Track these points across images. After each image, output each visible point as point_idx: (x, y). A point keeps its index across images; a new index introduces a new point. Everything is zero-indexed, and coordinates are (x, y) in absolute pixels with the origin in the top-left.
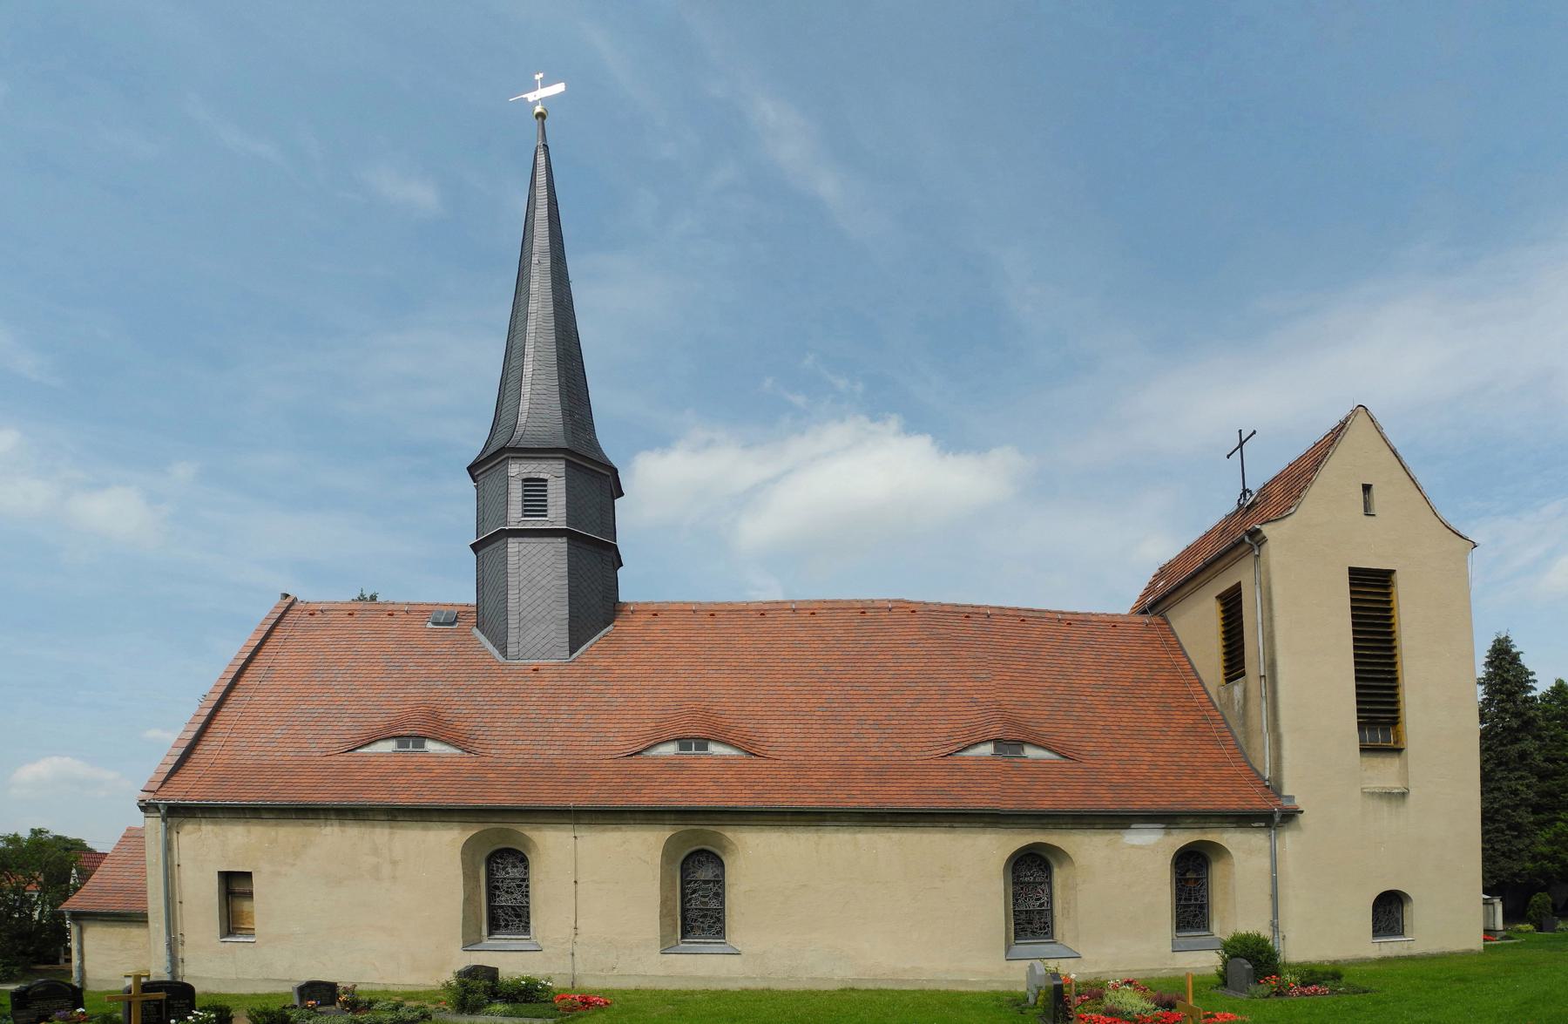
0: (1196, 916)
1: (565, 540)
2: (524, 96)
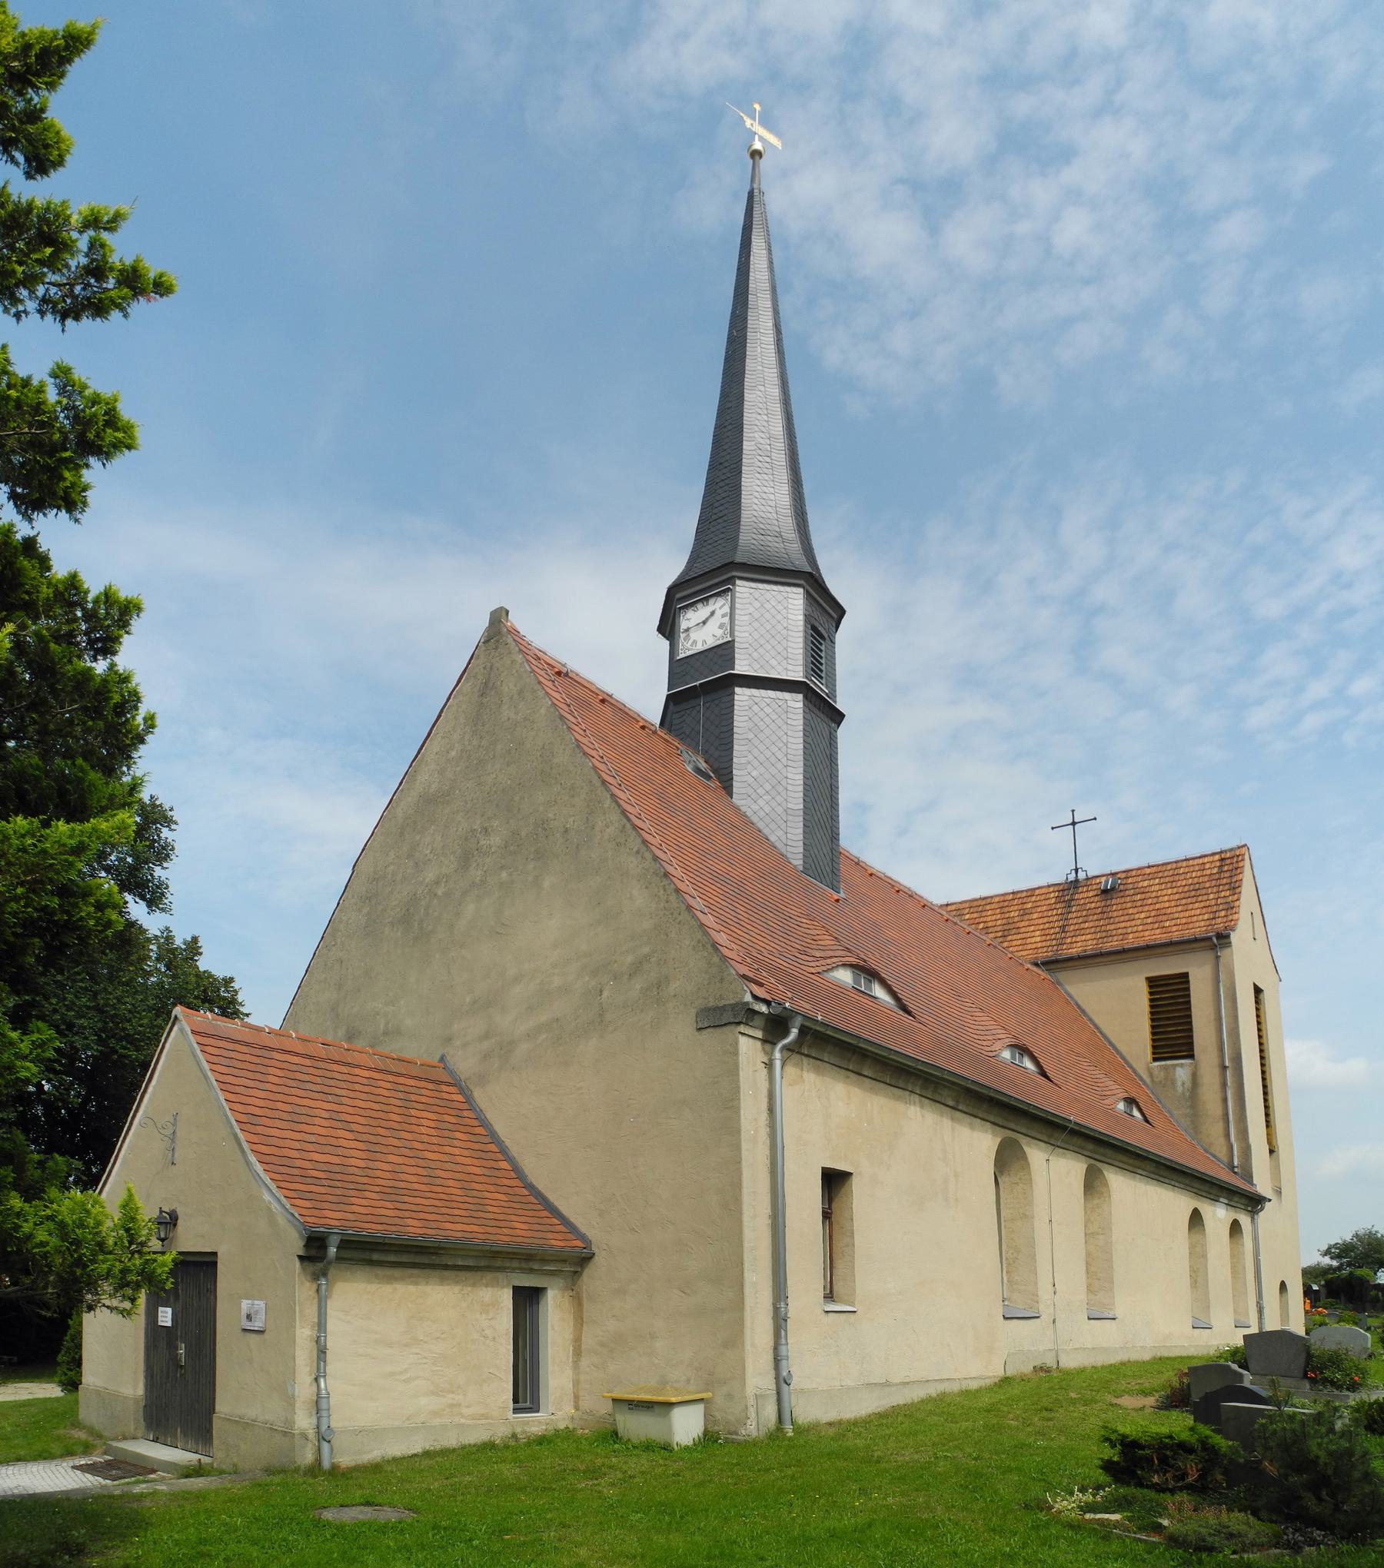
1: (800, 696)
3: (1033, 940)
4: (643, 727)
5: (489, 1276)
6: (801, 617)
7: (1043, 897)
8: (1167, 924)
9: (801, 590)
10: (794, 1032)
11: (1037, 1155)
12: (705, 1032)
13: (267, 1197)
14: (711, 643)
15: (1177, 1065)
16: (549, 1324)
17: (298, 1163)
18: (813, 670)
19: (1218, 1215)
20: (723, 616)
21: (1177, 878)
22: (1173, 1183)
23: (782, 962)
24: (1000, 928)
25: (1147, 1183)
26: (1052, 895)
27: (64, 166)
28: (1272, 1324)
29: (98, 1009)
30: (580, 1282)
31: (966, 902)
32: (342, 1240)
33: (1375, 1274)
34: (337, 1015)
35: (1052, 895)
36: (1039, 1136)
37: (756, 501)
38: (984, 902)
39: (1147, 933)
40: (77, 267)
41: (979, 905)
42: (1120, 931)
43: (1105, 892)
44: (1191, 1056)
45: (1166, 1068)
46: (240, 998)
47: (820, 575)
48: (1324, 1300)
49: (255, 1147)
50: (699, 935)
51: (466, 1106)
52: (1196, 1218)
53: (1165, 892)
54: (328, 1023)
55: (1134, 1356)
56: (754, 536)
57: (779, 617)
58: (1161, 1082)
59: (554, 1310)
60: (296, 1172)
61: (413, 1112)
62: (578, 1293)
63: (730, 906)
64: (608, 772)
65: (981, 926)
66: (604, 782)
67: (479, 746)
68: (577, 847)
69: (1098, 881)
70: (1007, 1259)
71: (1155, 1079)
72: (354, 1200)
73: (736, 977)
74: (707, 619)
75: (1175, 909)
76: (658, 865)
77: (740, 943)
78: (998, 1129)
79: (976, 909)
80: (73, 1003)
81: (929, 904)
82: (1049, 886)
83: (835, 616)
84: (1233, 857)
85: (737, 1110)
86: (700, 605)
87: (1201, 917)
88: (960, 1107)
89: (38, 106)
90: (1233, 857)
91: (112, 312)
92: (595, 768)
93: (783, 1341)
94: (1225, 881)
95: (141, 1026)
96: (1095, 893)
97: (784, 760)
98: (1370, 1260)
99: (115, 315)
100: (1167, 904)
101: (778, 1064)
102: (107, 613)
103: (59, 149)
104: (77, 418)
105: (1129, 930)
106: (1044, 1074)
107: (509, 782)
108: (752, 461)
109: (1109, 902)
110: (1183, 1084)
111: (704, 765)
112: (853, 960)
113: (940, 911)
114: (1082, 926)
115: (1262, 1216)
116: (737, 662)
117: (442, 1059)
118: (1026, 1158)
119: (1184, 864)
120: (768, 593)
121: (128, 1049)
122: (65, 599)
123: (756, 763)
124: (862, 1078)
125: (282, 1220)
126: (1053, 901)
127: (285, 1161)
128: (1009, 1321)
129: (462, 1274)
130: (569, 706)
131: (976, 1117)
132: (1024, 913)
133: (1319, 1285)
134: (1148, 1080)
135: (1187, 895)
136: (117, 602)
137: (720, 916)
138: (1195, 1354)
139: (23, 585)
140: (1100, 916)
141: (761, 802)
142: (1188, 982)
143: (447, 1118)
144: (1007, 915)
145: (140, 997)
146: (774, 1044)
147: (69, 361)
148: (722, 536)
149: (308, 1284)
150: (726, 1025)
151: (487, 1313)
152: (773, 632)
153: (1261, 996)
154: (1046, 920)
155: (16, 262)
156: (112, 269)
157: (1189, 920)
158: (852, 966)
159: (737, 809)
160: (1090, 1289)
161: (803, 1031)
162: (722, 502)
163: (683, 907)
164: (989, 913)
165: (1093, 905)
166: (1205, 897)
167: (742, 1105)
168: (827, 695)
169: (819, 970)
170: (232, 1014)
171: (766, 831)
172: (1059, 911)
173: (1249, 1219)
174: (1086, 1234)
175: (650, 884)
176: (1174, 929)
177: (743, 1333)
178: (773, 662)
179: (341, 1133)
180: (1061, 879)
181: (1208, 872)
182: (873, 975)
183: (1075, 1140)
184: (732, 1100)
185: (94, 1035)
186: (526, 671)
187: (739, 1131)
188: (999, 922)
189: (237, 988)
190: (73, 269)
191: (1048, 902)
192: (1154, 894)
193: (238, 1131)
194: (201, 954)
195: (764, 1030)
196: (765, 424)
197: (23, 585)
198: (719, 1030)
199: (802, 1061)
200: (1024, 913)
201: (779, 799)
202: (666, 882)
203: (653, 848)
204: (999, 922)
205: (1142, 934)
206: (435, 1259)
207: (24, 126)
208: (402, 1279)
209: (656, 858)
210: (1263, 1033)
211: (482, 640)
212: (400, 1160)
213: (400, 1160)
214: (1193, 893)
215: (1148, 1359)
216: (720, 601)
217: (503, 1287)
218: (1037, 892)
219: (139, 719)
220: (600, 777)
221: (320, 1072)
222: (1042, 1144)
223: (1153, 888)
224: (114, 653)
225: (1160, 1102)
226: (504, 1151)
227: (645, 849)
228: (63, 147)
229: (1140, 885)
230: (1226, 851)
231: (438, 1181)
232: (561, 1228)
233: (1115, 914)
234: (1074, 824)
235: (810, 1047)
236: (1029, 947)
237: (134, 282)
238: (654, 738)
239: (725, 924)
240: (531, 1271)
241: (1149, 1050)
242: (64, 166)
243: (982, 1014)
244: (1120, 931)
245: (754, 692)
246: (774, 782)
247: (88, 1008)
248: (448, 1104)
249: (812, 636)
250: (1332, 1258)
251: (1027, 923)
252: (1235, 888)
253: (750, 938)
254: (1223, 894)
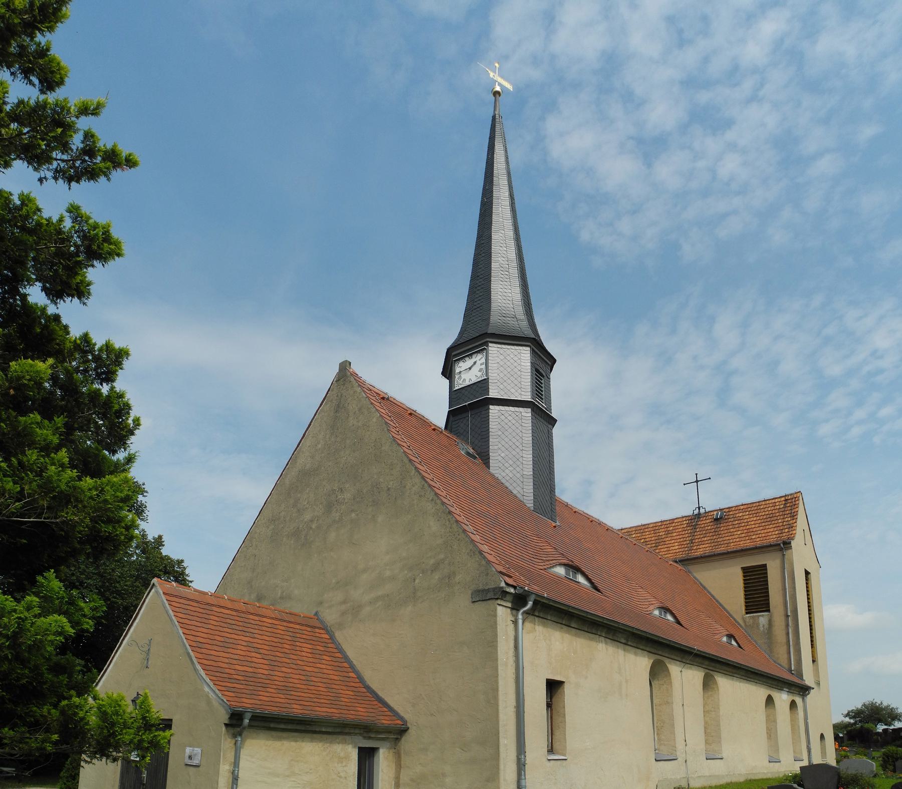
1: (529, 410)
3: (674, 548)
4: (434, 430)
5: (341, 737)
6: (529, 364)
7: (679, 524)
8: (754, 537)
9: (528, 349)
10: (530, 604)
11: (675, 669)
12: (477, 603)
13: (207, 689)
14: (474, 380)
15: (760, 615)
16: (380, 769)
17: (227, 671)
18: (537, 394)
19: (783, 698)
20: (481, 365)
21: (759, 511)
22: (756, 681)
23: (523, 563)
24: (654, 542)
25: (740, 682)
26: (685, 522)
27: (64, 85)
28: (817, 760)
29: (101, 575)
30: (399, 744)
31: (633, 527)
32: (252, 716)
33: (876, 726)
34: (251, 587)
35: (685, 522)
36: (676, 658)
37: (500, 297)
38: (644, 527)
39: (742, 543)
40: (77, 150)
41: (641, 529)
42: (725, 542)
43: (716, 520)
44: (768, 611)
45: (753, 617)
46: (187, 572)
47: (541, 340)
48: (846, 742)
49: (201, 661)
50: (471, 547)
51: (330, 641)
52: (770, 700)
53: (752, 519)
54: (246, 590)
55: (734, 780)
56: (499, 318)
57: (515, 364)
58: (750, 625)
59: (384, 762)
60: (225, 675)
61: (298, 644)
62: (398, 750)
63: (489, 530)
64: (414, 455)
65: (643, 541)
66: (410, 460)
67: (335, 441)
68: (395, 499)
69: (712, 514)
70: (657, 727)
71: (747, 624)
72: (261, 693)
73: (496, 573)
74: (472, 367)
75: (758, 529)
76: (452, 516)
77: (490, 545)
78: (651, 654)
79: (639, 531)
80: (85, 571)
81: (611, 529)
82: (683, 517)
83: (550, 363)
84: (792, 499)
85: (495, 647)
86: (467, 359)
87: (774, 533)
88: (629, 643)
89: (45, 47)
90: (792, 499)
91: (101, 177)
92: (405, 452)
93: (523, 777)
94: (788, 512)
95: (126, 586)
96: (711, 520)
97: (520, 447)
98: (873, 718)
99: (102, 179)
100: (753, 526)
101: (520, 621)
102: (108, 357)
103: (60, 74)
104: (85, 237)
105: (731, 541)
106: (678, 622)
107: (355, 462)
108: (497, 274)
109: (718, 526)
110: (764, 626)
111: (472, 450)
112: (565, 561)
113: (617, 532)
114: (703, 539)
115: (809, 698)
116: (490, 391)
117: (316, 614)
118: (668, 670)
119: (763, 503)
120: (508, 350)
121: (117, 598)
122: (81, 349)
123: (503, 449)
124: (570, 628)
125: (215, 703)
126: (685, 525)
127: (219, 669)
128: (659, 762)
129: (325, 736)
130: (380, 403)
131: (638, 648)
132: (668, 533)
133: (843, 734)
134: (743, 624)
135: (765, 520)
136: (114, 349)
137: (483, 536)
138: (771, 777)
139: (55, 339)
140: (713, 534)
141: (507, 471)
142: (766, 569)
143: (318, 647)
144: (658, 534)
145: (126, 569)
146: (518, 610)
147: (78, 202)
148: (480, 318)
149: (229, 740)
150: (489, 599)
151: (342, 762)
152: (512, 373)
153: (809, 576)
154: (681, 536)
155: (40, 139)
156: (99, 150)
157: (767, 535)
158: (565, 565)
159: (492, 475)
160: (707, 742)
161: (536, 603)
162: (480, 298)
163: (461, 531)
164: (647, 533)
165: (709, 527)
166: (776, 522)
167: (499, 645)
168: (546, 408)
169: (545, 567)
170: (181, 581)
171: (511, 488)
172: (689, 531)
173: (801, 700)
174: (704, 712)
175: (440, 518)
176: (758, 540)
177: (499, 773)
178: (512, 390)
179: (253, 654)
180: (691, 513)
181: (778, 507)
182: (577, 570)
183: (697, 659)
184: (493, 642)
185: (97, 590)
186: (363, 397)
187: (497, 660)
188: (653, 539)
189: (185, 566)
190: (75, 150)
191: (682, 526)
192: (746, 521)
193: (190, 651)
194: (163, 545)
195: (512, 602)
196: (505, 252)
197: (55, 339)
198: (485, 602)
199: (534, 618)
200: (668, 533)
201: (518, 469)
202: (450, 517)
203: (442, 498)
204: (653, 539)
205: (739, 543)
206: (309, 728)
207: (37, 60)
208: (287, 738)
209: (443, 503)
210: (810, 596)
211: (335, 380)
212: (289, 671)
213: (289, 671)
214: (769, 519)
215: (743, 781)
216: (480, 356)
217: (349, 744)
218: (676, 521)
219: (130, 421)
220: (408, 457)
221: (242, 619)
222: (678, 663)
223: (745, 517)
224: (113, 381)
225: (750, 636)
226: (352, 667)
227: (437, 498)
228: (63, 72)
229: (737, 515)
230: (788, 495)
231: (312, 683)
232: (389, 713)
233: (722, 532)
234: (697, 481)
235: (539, 612)
236: (672, 552)
237: (114, 159)
238: (441, 436)
239: (487, 540)
240: (370, 738)
241: (744, 608)
242: (64, 85)
243: (641, 590)
244: (725, 542)
245: (501, 408)
246: (515, 460)
247: (94, 574)
248: (319, 640)
249: (536, 375)
250: (850, 718)
251: (670, 539)
252: (794, 516)
253: (477, 511)
254: (787, 519)
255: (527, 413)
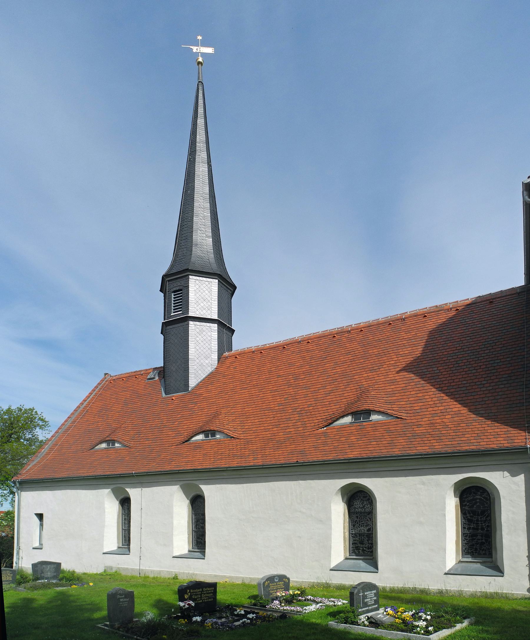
0: (482, 544)
1: (216, 325)
2: (191, 47)
9: (217, 281)
83: (232, 290)
255: (215, 326)
